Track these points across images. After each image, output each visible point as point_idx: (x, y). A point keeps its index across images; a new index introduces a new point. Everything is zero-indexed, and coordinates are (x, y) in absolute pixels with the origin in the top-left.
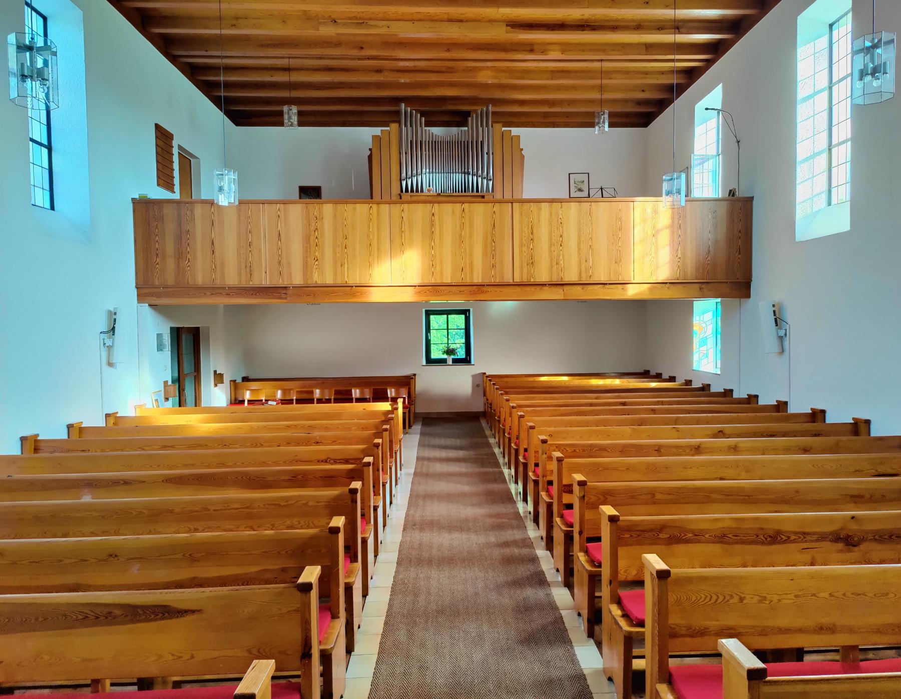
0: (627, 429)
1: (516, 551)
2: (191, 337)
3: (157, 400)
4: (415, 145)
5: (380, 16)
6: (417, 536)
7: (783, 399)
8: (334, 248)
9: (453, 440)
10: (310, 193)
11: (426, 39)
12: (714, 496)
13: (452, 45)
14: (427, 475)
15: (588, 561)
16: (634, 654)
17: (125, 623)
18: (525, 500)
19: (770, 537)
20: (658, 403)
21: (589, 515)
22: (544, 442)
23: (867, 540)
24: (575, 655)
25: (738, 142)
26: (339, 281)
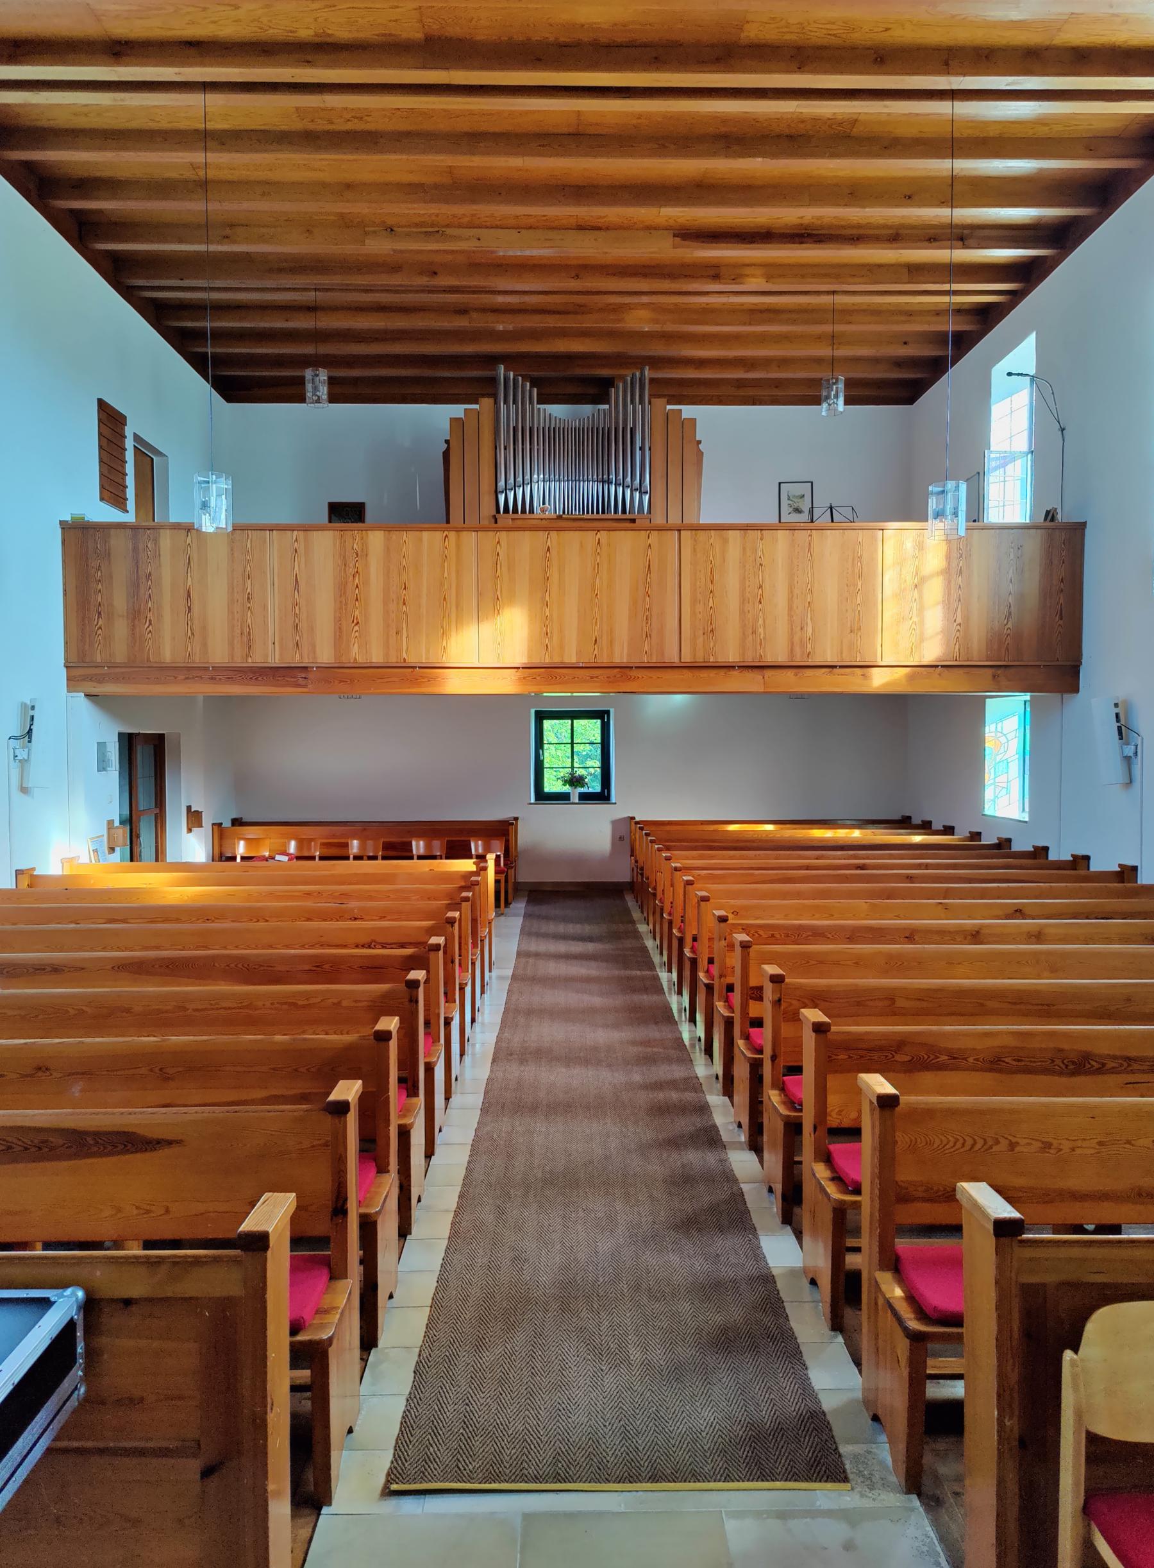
0: (862, 904)
1: (674, 1096)
2: (150, 749)
3: (95, 851)
4: (522, 434)
5: (465, 220)
6: (514, 1071)
7: (1130, 862)
9: (578, 926)
10: (347, 513)
11: (541, 258)
12: (991, 1004)
13: (583, 269)
14: (534, 980)
15: (784, 1103)
16: (849, 1244)
17: (70, 1158)
18: (692, 1020)
19: (1073, 1063)
20: (919, 866)
21: (787, 1030)
22: (723, 919)
24: (759, 1247)
25: (1063, 430)
26: (393, 660)
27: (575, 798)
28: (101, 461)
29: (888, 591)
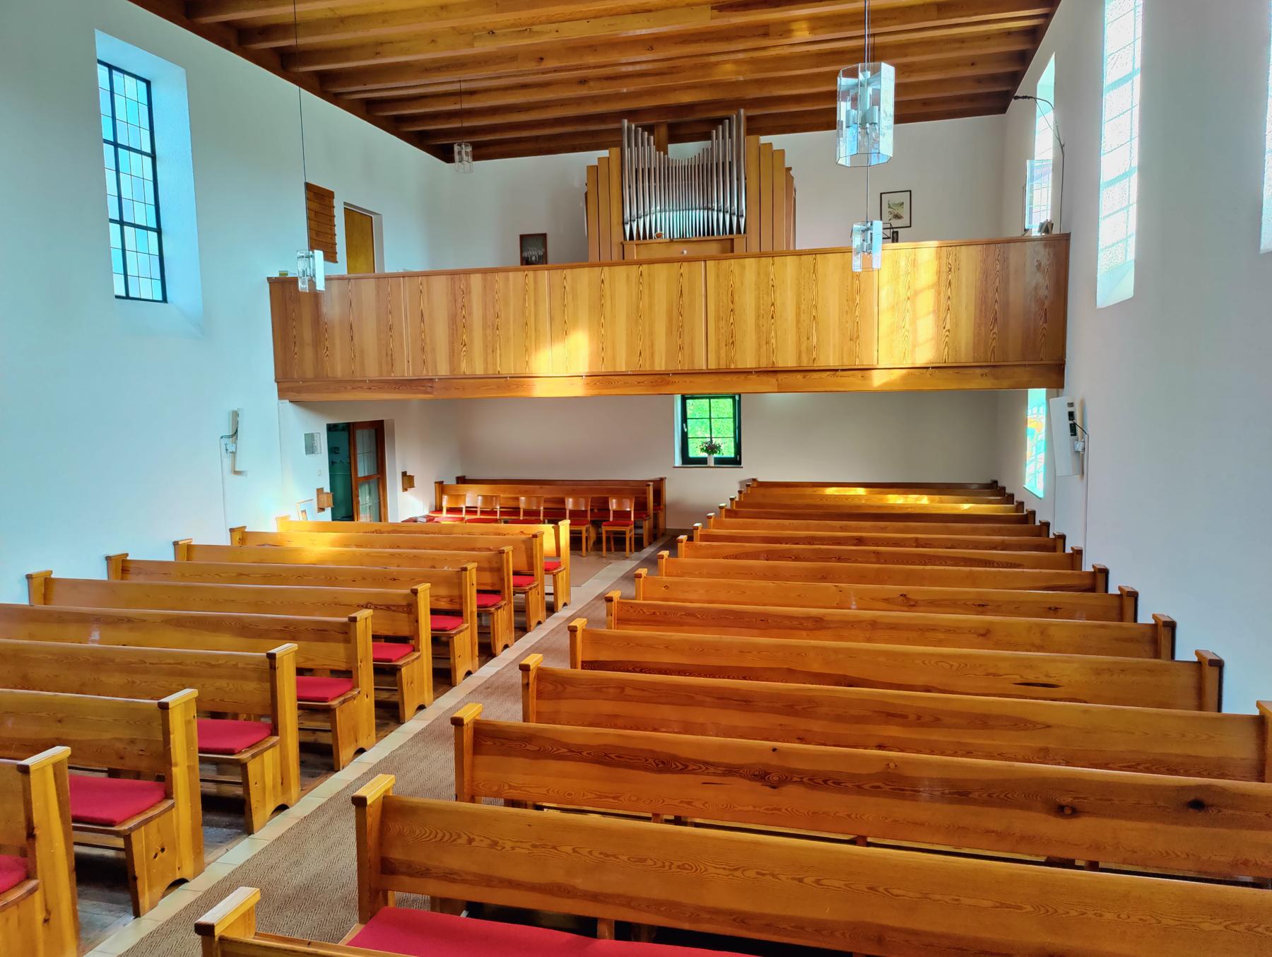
8: (484, 328)
23: (791, 782)
26: (491, 372)
27: (711, 463)
28: (310, 229)
29: (884, 304)
